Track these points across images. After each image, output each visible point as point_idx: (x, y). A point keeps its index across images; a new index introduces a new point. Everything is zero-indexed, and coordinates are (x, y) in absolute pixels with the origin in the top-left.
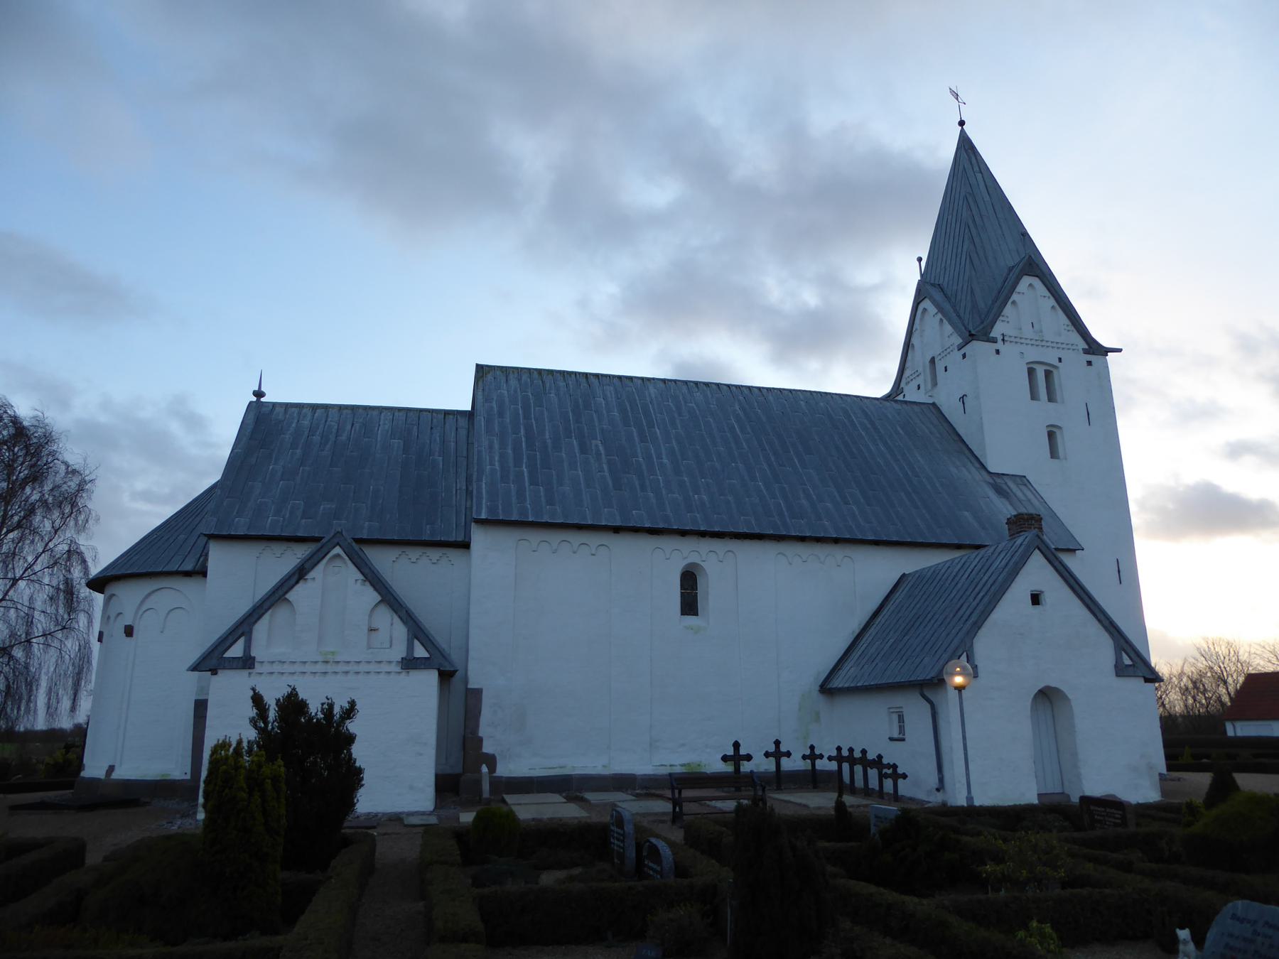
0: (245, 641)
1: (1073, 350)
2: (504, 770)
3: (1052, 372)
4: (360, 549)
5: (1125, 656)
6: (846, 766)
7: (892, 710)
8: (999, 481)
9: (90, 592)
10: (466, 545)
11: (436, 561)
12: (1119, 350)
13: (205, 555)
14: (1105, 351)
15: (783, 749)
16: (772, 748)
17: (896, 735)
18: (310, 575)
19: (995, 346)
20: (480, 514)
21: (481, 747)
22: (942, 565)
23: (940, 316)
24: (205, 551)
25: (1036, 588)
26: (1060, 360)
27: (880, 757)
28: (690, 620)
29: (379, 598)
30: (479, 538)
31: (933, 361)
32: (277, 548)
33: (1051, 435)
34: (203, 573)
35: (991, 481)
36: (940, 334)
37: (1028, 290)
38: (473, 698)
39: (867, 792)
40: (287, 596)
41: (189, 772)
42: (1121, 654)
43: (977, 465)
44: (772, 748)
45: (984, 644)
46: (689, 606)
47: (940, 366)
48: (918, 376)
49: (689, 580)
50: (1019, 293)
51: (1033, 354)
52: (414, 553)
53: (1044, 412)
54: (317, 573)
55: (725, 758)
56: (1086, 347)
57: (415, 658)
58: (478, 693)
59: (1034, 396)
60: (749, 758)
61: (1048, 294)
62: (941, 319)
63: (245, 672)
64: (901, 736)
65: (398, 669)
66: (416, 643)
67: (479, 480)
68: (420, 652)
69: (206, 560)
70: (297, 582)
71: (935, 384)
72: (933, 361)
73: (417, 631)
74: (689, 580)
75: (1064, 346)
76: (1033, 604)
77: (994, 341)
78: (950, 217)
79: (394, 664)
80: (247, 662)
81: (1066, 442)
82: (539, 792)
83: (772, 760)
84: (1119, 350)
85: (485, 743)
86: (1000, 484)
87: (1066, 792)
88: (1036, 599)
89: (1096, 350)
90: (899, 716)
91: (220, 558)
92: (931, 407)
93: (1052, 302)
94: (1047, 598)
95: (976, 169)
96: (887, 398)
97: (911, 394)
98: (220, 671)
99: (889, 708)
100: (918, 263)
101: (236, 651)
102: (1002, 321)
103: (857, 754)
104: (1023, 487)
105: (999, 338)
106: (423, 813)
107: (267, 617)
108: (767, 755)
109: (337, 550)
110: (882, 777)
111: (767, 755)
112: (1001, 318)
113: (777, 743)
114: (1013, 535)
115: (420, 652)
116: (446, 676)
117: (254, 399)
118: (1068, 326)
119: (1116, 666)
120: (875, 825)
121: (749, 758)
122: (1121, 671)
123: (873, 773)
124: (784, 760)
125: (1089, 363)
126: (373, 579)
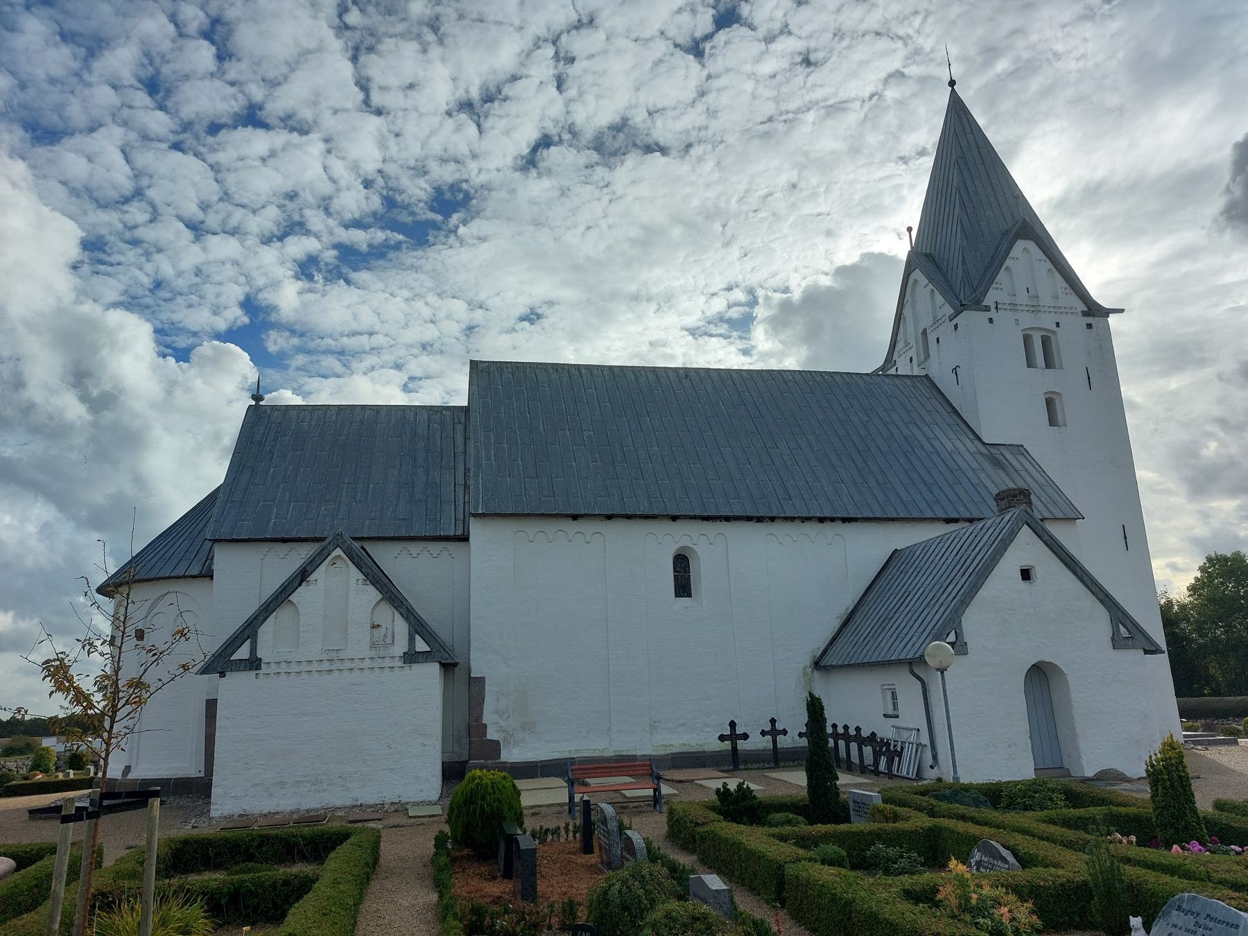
0: (251, 644)
1: (1072, 313)
2: (511, 755)
3: (1049, 337)
4: (362, 548)
5: (1122, 629)
6: (841, 743)
7: (885, 687)
8: (993, 451)
9: (306, 395)
10: (465, 539)
11: (436, 555)
12: (1121, 311)
13: (210, 558)
14: (1106, 313)
15: (779, 726)
16: (768, 728)
17: (890, 712)
18: (312, 578)
19: (989, 315)
20: (477, 508)
21: (485, 734)
22: (931, 542)
23: (931, 286)
24: (211, 555)
25: (1026, 563)
26: (1058, 325)
27: (873, 734)
28: (684, 601)
29: (381, 596)
30: (478, 531)
31: (924, 333)
32: (282, 549)
33: (1050, 403)
34: (210, 576)
35: (987, 452)
36: (930, 302)
37: (1023, 253)
38: (476, 686)
39: (863, 770)
40: (290, 598)
41: (203, 771)
42: (1118, 627)
43: (971, 436)
44: (768, 728)
45: (973, 622)
46: (683, 588)
47: (932, 338)
48: (910, 348)
49: (682, 563)
50: (1013, 258)
51: (1027, 320)
52: (415, 548)
53: (1043, 380)
54: (319, 574)
55: (722, 738)
56: (1086, 309)
57: (416, 652)
58: (481, 680)
59: (1030, 363)
60: (745, 736)
61: (1045, 258)
62: (932, 290)
63: (253, 673)
64: (895, 713)
65: (401, 664)
66: (418, 637)
67: (476, 476)
68: (421, 646)
69: (211, 563)
70: (300, 585)
71: (927, 356)
72: (924, 333)
73: (418, 626)
74: (682, 563)
75: (1062, 310)
76: (1030, 579)
77: (987, 309)
78: (941, 183)
79: (397, 659)
80: (254, 663)
81: (1069, 409)
82: (543, 776)
83: (769, 738)
84: (1121, 311)
85: (489, 730)
86: (995, 455)
87: (1066, 766)
88: (1026, 574)
89: (1095, 312)
90: (893, 693)
91: (225, 560)
92: (924, 379)
93: (1049, 265)
94: (1038, 573)
95: (968, 130)
96: (875, 374)
97: (903, 368)
98: (228, 674)
99: (882, 685)
100: (908, 233)
101: (243, 653)
102: (996, 288)
103: (852, 732)
104: (1020, 457)
105: (993, 306)
106: (430, 803)
107: (272, 618)
108: (763, 733)
109: (338, 552)
110: (877, 755)
111: (763, 733)
112: (994, 285)
113: (773, 721)
114: (1002, 511)
115: (421, 646)
116: (448, 668)
117: (253, 403)
118: (1065, 289)
119: (1113, 639)
120: (854, 810)
121: (745, 736)
122: (1117, 643)
123: (868, 751)
124: (780, 738)
125: (1089, 326)
126: (376, 577)
